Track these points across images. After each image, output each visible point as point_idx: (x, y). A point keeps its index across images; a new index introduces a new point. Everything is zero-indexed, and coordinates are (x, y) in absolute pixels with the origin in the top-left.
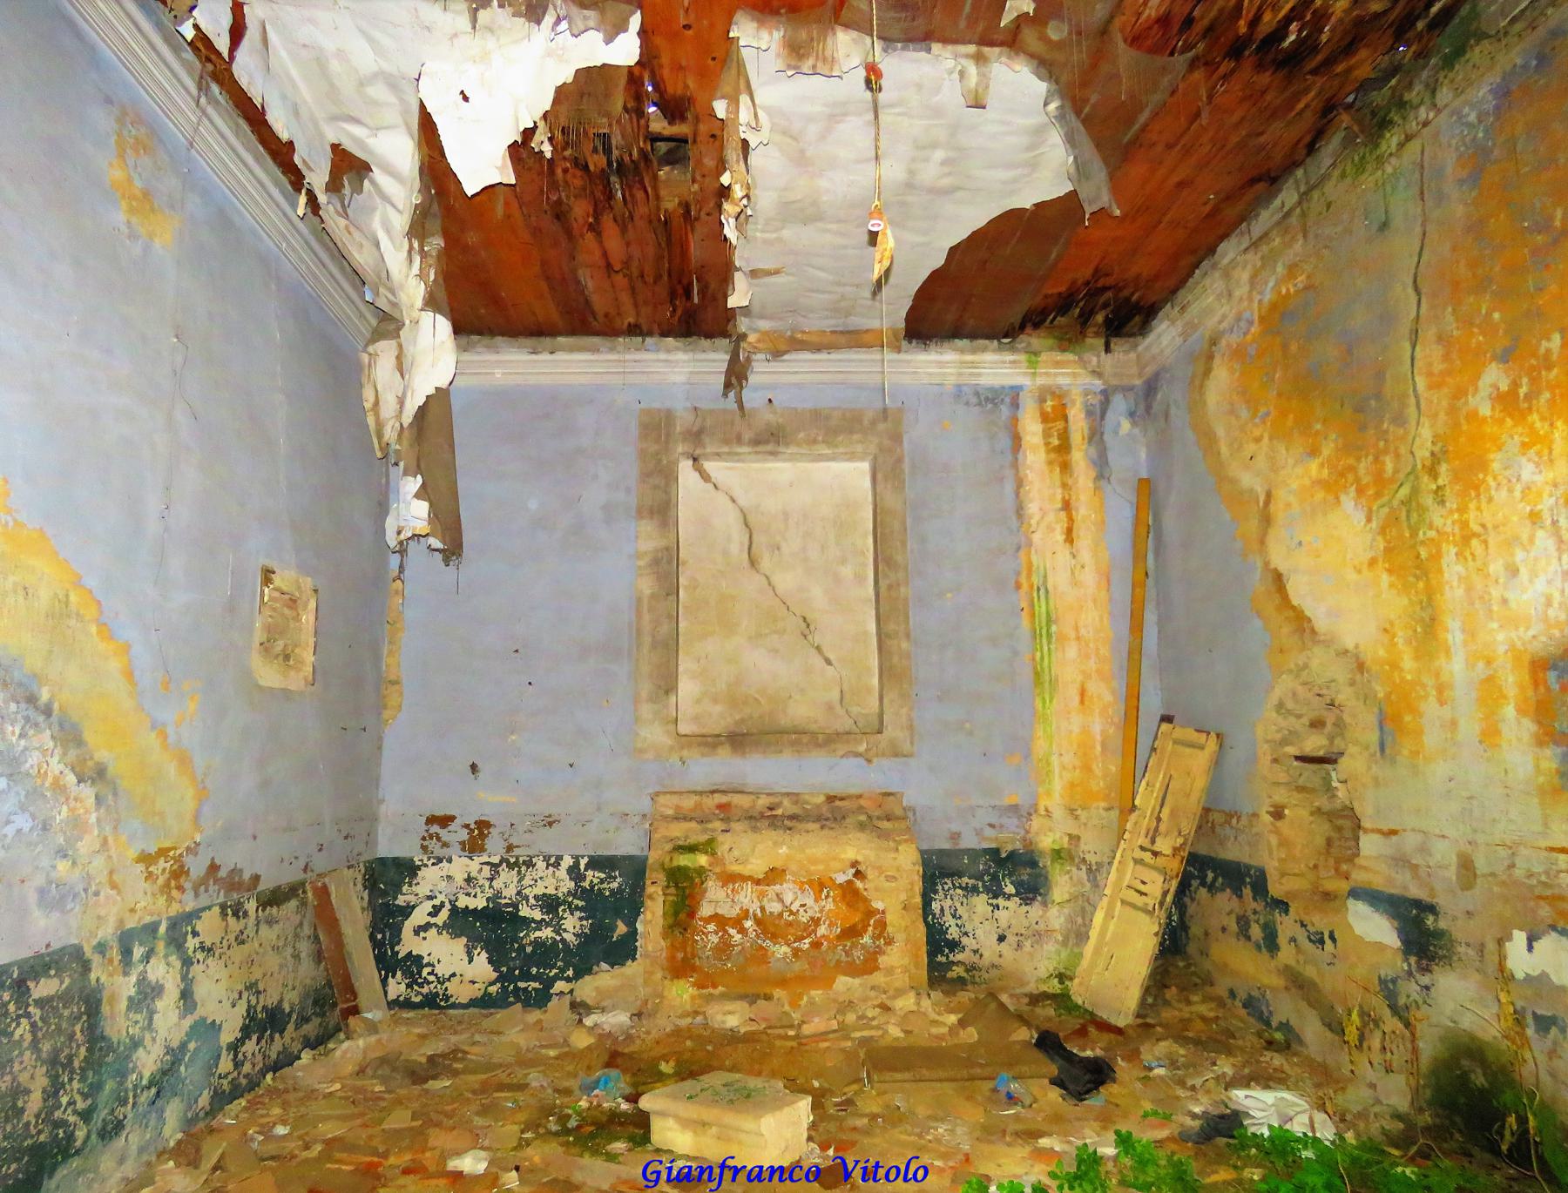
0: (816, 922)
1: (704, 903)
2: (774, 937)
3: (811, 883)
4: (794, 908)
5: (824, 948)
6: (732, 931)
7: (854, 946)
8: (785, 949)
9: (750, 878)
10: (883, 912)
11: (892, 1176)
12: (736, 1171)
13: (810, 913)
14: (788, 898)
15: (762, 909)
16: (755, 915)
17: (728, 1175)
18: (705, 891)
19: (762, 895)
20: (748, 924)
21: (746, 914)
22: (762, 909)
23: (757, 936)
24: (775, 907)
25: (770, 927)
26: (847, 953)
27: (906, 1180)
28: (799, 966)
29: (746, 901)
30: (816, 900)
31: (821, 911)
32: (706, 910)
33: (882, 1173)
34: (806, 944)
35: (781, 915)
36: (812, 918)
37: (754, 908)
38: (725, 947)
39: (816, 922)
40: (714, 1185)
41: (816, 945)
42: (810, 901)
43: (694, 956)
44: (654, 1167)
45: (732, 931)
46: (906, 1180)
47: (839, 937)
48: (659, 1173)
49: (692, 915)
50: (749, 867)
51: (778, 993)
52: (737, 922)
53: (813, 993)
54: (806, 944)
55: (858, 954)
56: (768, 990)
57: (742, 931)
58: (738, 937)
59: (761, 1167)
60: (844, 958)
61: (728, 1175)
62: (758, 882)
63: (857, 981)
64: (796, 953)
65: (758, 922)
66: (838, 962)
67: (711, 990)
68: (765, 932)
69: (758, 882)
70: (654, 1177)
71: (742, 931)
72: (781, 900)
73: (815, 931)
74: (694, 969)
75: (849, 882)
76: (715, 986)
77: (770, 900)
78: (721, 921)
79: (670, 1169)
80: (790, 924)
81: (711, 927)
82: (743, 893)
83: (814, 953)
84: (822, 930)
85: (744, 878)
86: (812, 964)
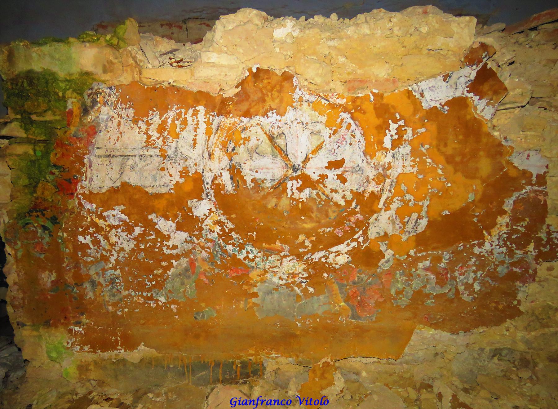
0: (368, 204)
1: (93, 158)
2: (265, 238)
3: (355, 108)
4: (313, 170)
5: (384, 265)
6: (165, 226)
7: (459, 259)
8: (290, 265)
9: (202, 97)
10: (541, 180)
11: (316, 403)
12: (263, 401)
13: (354, 182)
14: (299, 146)
15: (235, 172)
16: (218, 188)
17: (260, 402)
18: (93, 131)
19: (231, 142)
20: (202, 208)
21: (195, 185)
22: (235, 172)
23: (225, 236)
24: (265, 169)
25: (250, 212)
26: (442, 279)
27: (321, 404)
28: (328, 304)
29: (195, 154)
30: (368, 153)
31: (380, 179)
32: (99, 176)
33: (313, 402)
34: (340, 255)
35: (280, 187)
36: (358, 195)
37: (216, 168)
38: (148, 263)
39: (368, 204)
40: (255, 406)
41: (367, 257)
42: (352, 153)
43: (79, 280)
44: (234, 400)
45: (165, 226)
46: (321, 404)
47: (421, 241)
48: (236, 402)
49: (67, 185)
50: (203, 73)
51: (276, 361)
52: (177, 206)
53: (355, 362)
54: (340, 255)
55: (469, 279)
56: (250, 355)
57: (189, 223)
58: (179, 238)
59: (271, 400)
60: (433, 289)
61: (260, 402)
62: (220, 106)
63: (461, 339)
64: (316, 272)
65: (224, 202)
66: (419, 296)
67: (122, 353)
68: (243, 226)
69: (220, 106)
70: (234, 403)
71: (189, 223)
72: (281, 152)
73: (363, 225)
74: (82, 306)
75: (458, 104)
76: (130, 343)
77: (255, 152)
78: (138, 203)
79: (240, 401)
80: (304, 210)
81: (116, 215)
82: (187, 135)
83: (363, 276)
84: (382, 223)
85: (189, 99)
86: (357, 302)
